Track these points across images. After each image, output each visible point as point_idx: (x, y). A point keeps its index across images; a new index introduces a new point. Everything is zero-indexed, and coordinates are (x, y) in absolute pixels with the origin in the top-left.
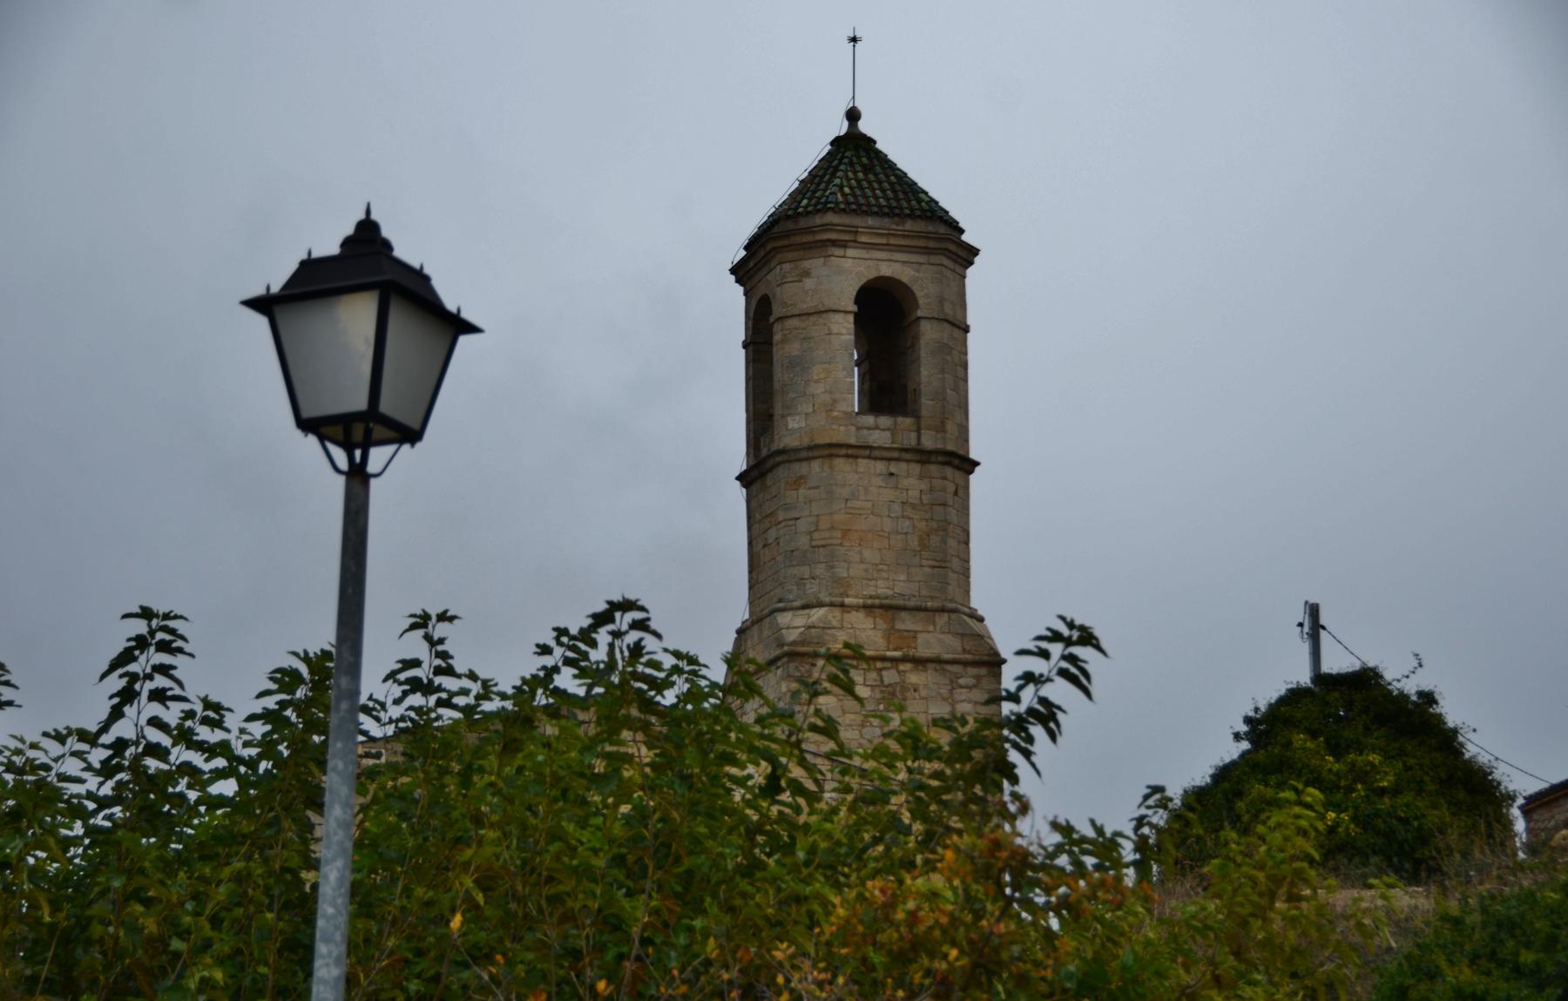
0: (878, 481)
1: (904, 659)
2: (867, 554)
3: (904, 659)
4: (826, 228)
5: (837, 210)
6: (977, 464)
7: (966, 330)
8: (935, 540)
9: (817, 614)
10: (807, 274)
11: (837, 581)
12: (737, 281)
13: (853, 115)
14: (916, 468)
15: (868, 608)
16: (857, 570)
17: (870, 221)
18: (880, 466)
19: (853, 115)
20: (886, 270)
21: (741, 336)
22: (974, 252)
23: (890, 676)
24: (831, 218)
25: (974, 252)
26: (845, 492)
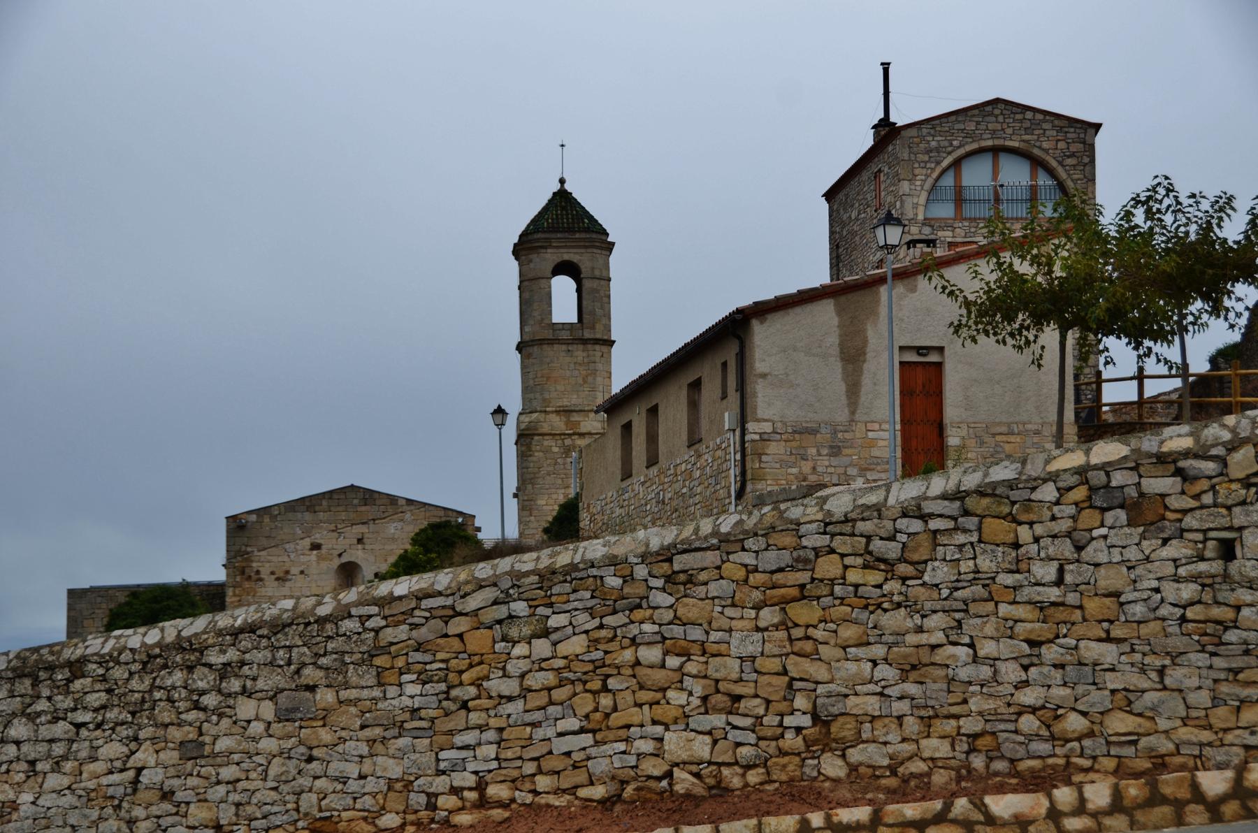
0: (563, 354)
1: (574, 434)
2: (558, 387)
3: (574, 434)
4: (538, 240)
5: (544, 232)
6: (1097, 127)
7: (609, 280)
8: (590, 379)
9: (535, 415)
10: (531, 261)
11: (544, 400)
12: (515, 245)
13: (562, 181)
14: (581, 347)
15: (557, 412)
16: (554, 395)
17: (559, 235)
18: (564, 347)
19: (562, 181)
20: (566, 257)
21: (190, 579)
22: (613, 244)
23: (568, 442)
24: (540, 235)
25: (613, 244)
26: (548, 360)
